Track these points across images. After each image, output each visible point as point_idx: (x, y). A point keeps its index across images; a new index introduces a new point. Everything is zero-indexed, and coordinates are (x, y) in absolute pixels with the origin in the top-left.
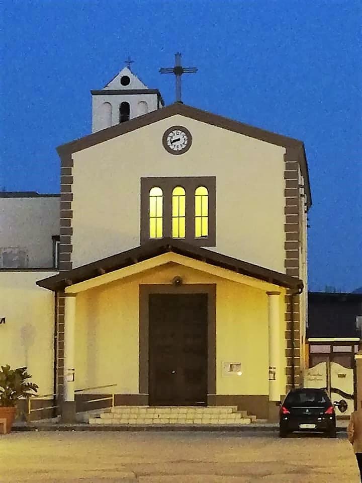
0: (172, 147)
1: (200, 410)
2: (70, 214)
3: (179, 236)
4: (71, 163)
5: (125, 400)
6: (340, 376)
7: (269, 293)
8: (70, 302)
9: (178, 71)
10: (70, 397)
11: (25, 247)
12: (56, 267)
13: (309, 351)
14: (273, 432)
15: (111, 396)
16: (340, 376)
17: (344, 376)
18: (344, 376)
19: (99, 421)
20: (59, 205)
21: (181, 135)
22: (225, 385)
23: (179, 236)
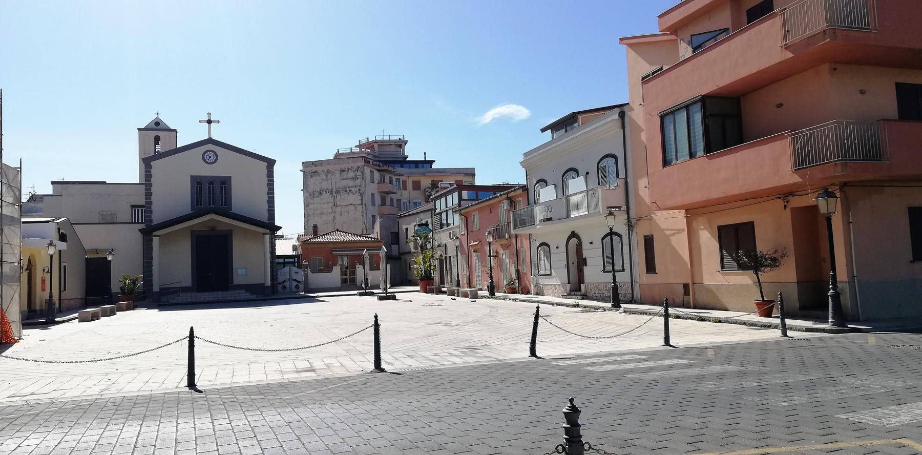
0: (209, 161)
1: (224, 293)
2: (151, 194)
3: (425, 158)
4: (151, 167)
5: (185, 290)
6: (296, 273)
7: (264, 234)
8: (156, 241)
9: (209, 122)
10: (156, 288)
11: (782, 47)
12: (140, 221)
13: (399, 246)
14: (364, 291)
15: (179, 287)
16: (296, 273)
17: (297, 273)
18: (297, 273)
19: (174, 301)
20: (144, 189)
21: (212, 155)
22: (237, 281)
23: (425, 158)
